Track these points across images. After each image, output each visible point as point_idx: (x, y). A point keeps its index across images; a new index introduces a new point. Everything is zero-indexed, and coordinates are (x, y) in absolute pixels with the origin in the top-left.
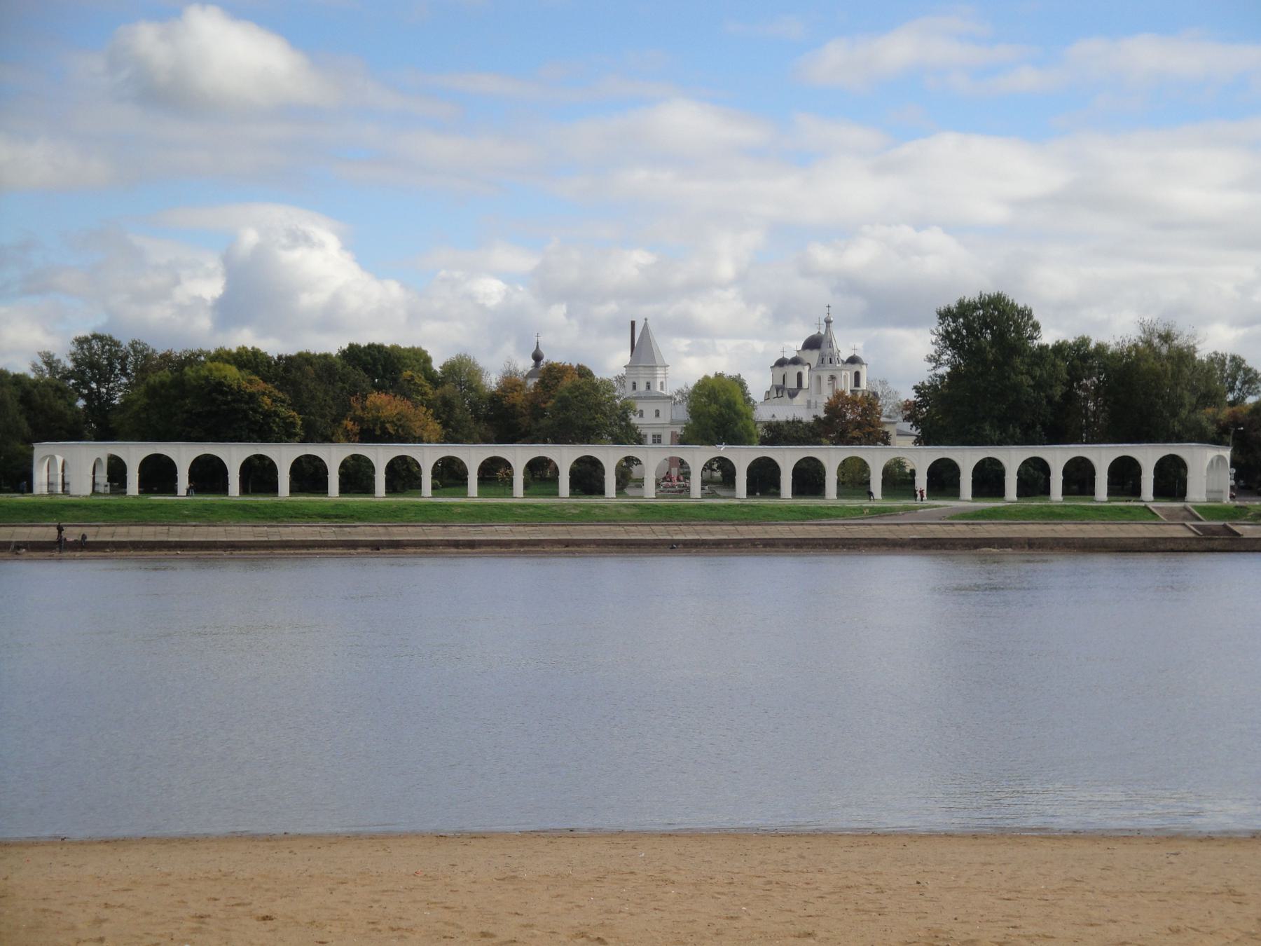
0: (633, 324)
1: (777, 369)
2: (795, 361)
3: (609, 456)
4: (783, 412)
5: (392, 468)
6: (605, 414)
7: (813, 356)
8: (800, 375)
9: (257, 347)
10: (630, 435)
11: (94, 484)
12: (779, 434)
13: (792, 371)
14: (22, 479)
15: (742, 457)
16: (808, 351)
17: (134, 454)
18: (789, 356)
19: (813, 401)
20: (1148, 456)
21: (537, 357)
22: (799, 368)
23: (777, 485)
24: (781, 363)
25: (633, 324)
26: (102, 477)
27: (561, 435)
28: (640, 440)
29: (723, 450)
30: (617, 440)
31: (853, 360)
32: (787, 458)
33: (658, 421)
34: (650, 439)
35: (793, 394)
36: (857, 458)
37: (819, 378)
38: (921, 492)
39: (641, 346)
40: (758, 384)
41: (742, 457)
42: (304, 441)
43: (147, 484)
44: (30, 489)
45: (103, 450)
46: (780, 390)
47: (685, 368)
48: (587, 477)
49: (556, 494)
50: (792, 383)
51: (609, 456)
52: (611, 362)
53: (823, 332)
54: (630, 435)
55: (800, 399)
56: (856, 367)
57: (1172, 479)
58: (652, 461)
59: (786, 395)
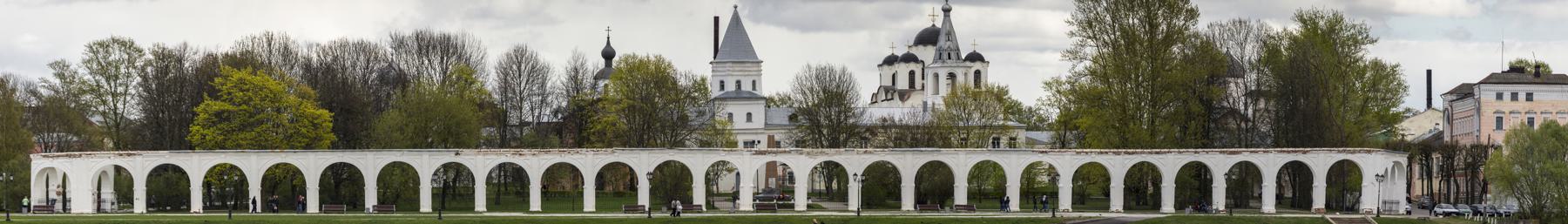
0: (716, 20)
1: (886, 67)
2: (909, 58)
3: (697, 162)
4: (898, 112)
5: (384, 177)
6: (181, 100)
7: (927, 53)
8: (912, 74)
9: (667, 57)
10: (716, 137)
11: (99, 201)
12: (908, 137)
13: (903, 70)
14: (16, 196)
15: (855, 162)
16: (921, 47)
17: (141, 165)
18: (899, 53)
19: (930, 103)
20: (1320, 162)
21: (608, 54)
22: (912, 66)
23: (898, 197)
24: (890, 61)
25: (716, 20)
26: (108, 193)
27: (640, 139)
28: (732, 145)
29: (1246, 156)
30: (705, 144)
31: (975, 57)
32: (908, 164)
33: (749, 126)
34: (741, 145)
35: (903, 96)
36: (345, 164)
37: (936, 76)
38: (254, 202)
39: (732, 44)
40: (866, 85)
41: (855, 162)
42: (334, 147)
43: (1080, 200)
44: (188, 209)
45: (105, 161)
46: (889, 92)
47: (783, 64)
48: (671, 183)
49: (472, 209)
50: (903, 84)
51: (697, 162)
52: (691, 61)
53: (939, 25)
54: (716, 137)
55: (915, 100)
56: (977, 66)
57: (1345, 181)
58: (749, 169)
59: (896, 96)
